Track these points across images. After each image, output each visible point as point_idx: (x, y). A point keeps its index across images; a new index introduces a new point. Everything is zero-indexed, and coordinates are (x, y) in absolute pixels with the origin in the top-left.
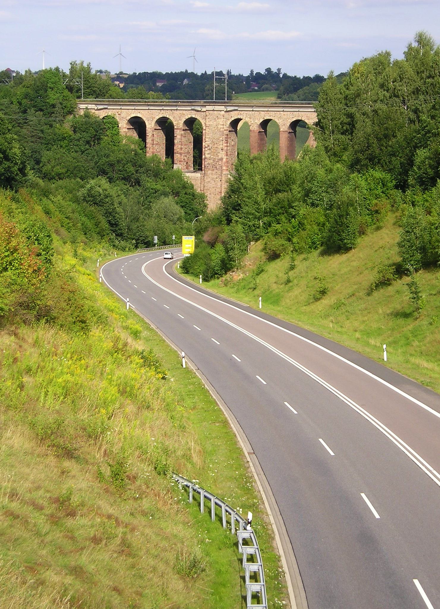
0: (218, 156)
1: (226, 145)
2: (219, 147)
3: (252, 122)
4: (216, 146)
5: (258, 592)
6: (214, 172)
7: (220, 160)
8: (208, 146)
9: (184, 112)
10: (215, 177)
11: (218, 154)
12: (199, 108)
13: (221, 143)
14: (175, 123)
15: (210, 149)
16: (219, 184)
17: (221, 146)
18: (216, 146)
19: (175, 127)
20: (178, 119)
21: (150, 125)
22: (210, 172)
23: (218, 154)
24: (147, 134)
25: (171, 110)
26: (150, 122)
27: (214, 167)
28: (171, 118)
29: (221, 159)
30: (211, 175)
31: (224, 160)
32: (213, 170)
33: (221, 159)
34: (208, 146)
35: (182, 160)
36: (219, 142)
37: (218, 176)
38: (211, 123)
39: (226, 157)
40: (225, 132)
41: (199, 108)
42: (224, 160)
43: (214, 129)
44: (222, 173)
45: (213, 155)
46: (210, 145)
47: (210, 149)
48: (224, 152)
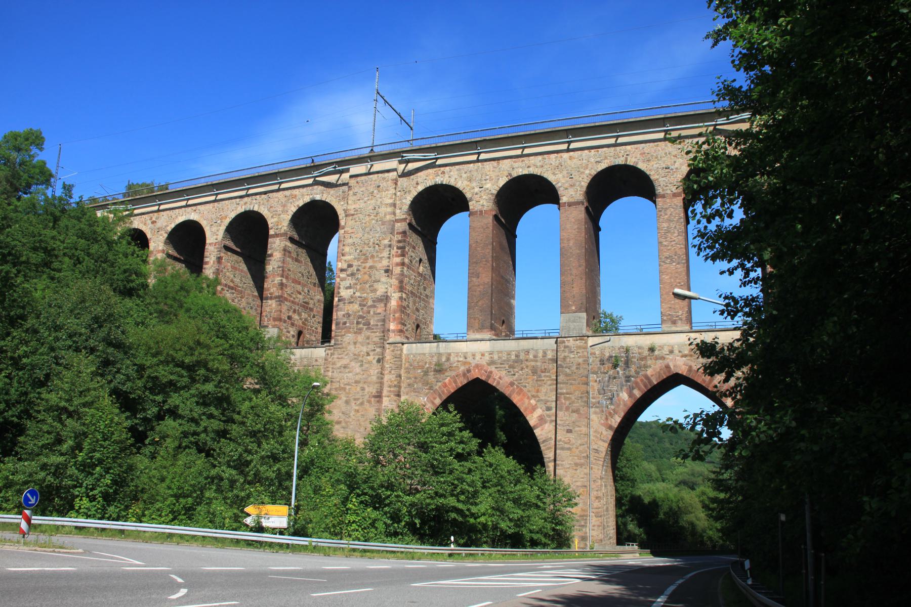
0: (375, 291)
1: (398, 260)
2: (379, 265)
3: (477, 190)
4: (370, 263)
5: (569, 547)
6: (360, 338)
7: (379, 300)
8: (350, 266)
9: (296, 192)
10: (365, 349)
11: (376, 285)
12: (332, 179)
13: (385, 254)
14: (271, 222)
15: (352, 275)
16: (374, 370)
17: (385, 262)
18: (370, 263)
19: (271, 232)
20: (280, 209)
21: (215, 235)
22: (349, 337)
23: (376, 285)
24: (206, 260)
25: (265, 193)
26: (214, 229)
27: (363, 322)
28: (264, 212)
29: (386, 299)
30: (351, 347)
31: (393, 303)
32: (359, 332)
33: (386, 299)
34: (350, 266)
35: (284, 317)
36: (381, 251)
37: (371, 347)
38: (361, 204)
39: (399, 294)
40: (398, 225)
41: (332, 179)
42: (393, 303)
43: (367, 219)
44: (383, 339)
45: (362, 290)
46: (355, 263)
47: (352, 275)
48: (394, 282)
